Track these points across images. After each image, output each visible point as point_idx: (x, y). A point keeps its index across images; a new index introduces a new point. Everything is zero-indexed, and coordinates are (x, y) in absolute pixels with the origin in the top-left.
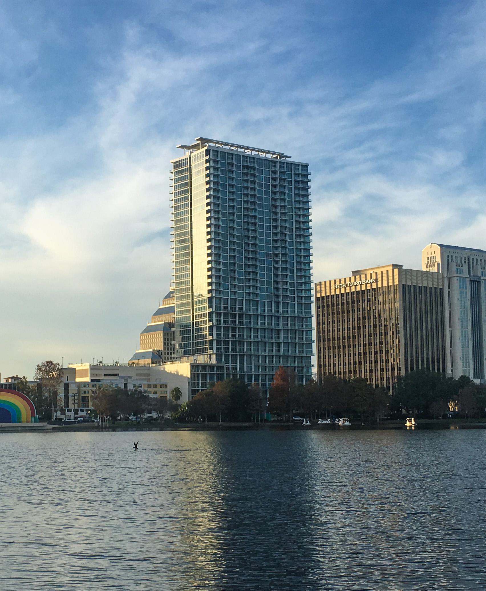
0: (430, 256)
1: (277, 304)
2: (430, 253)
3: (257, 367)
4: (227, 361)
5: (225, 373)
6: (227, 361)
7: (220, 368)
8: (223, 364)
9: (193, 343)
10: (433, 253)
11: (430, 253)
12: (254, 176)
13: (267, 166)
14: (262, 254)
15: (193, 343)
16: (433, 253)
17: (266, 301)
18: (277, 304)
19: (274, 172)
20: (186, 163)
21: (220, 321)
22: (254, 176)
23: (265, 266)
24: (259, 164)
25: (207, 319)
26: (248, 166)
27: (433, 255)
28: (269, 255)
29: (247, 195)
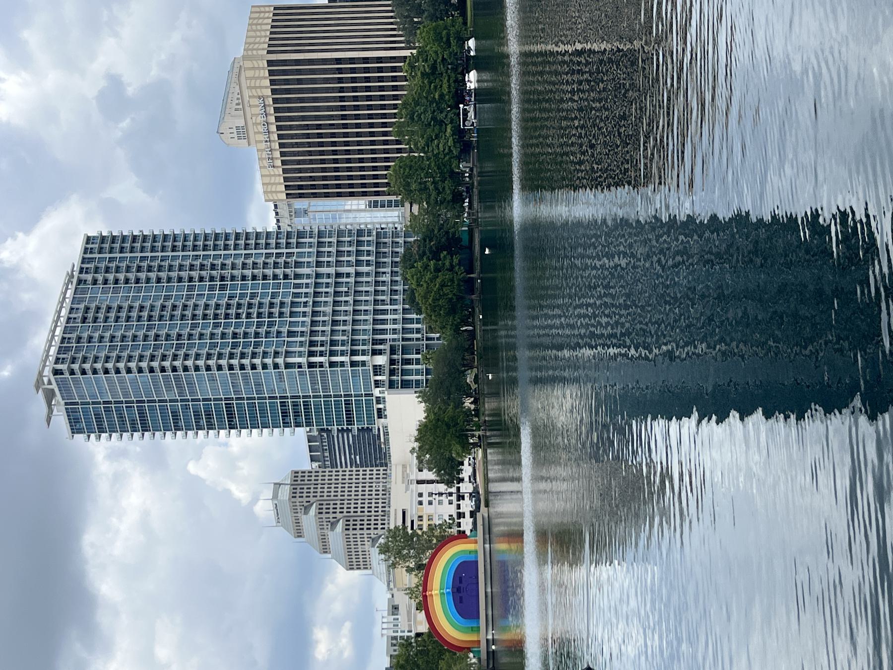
0: (235, 135)
1: (297, 276)
2: (232, 135)
3: (393, 302)
4: (382, 342)
5: (401, 343)
6: (382, 342)
7: (393, 351)
8: (386, 347)
9: (259, 398)
10: (231, 131)
11: (232, 135)
12: (98, 309)
13: (84, 292)
14: (220, 297)
15: (259, 398)
16: (231, 131)
17: (292, 290)
18: (297, 276)
19: (95, 282)
20: (75, 411)
21: (363, 351)
22: (98, 309)
23: (185, 293)
24: (80, 301)
25: (360, 368)
26: (83, 316)
27: (234, 130)
28: (191, 289)
29: (106, 319)
